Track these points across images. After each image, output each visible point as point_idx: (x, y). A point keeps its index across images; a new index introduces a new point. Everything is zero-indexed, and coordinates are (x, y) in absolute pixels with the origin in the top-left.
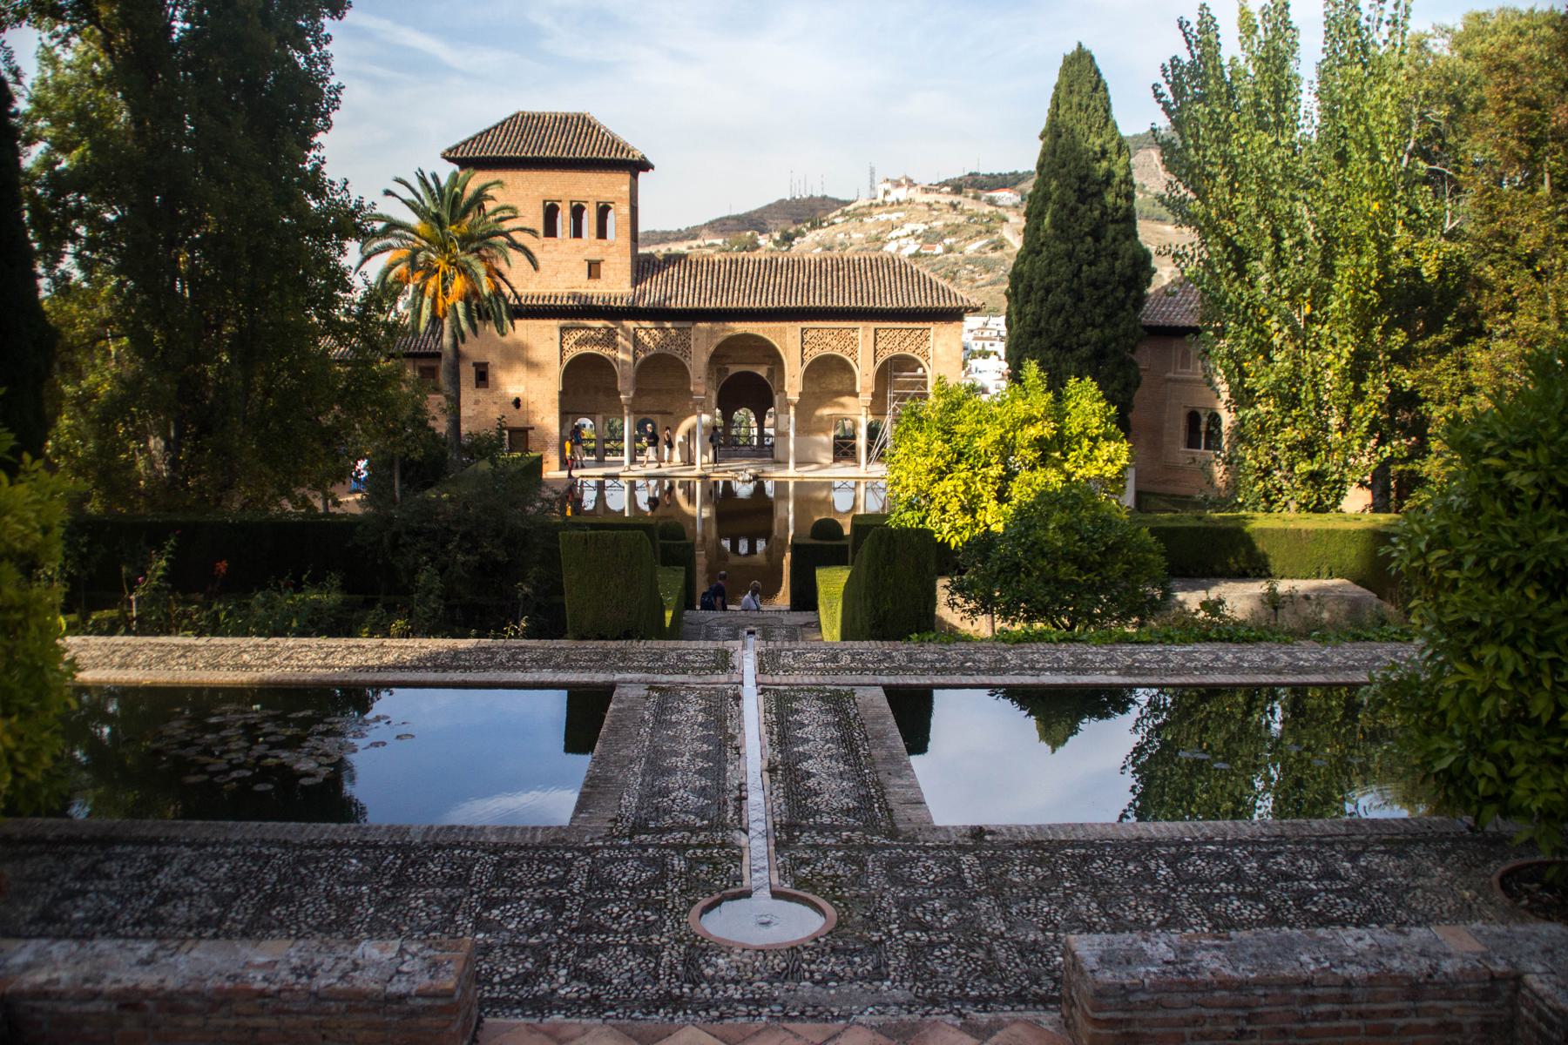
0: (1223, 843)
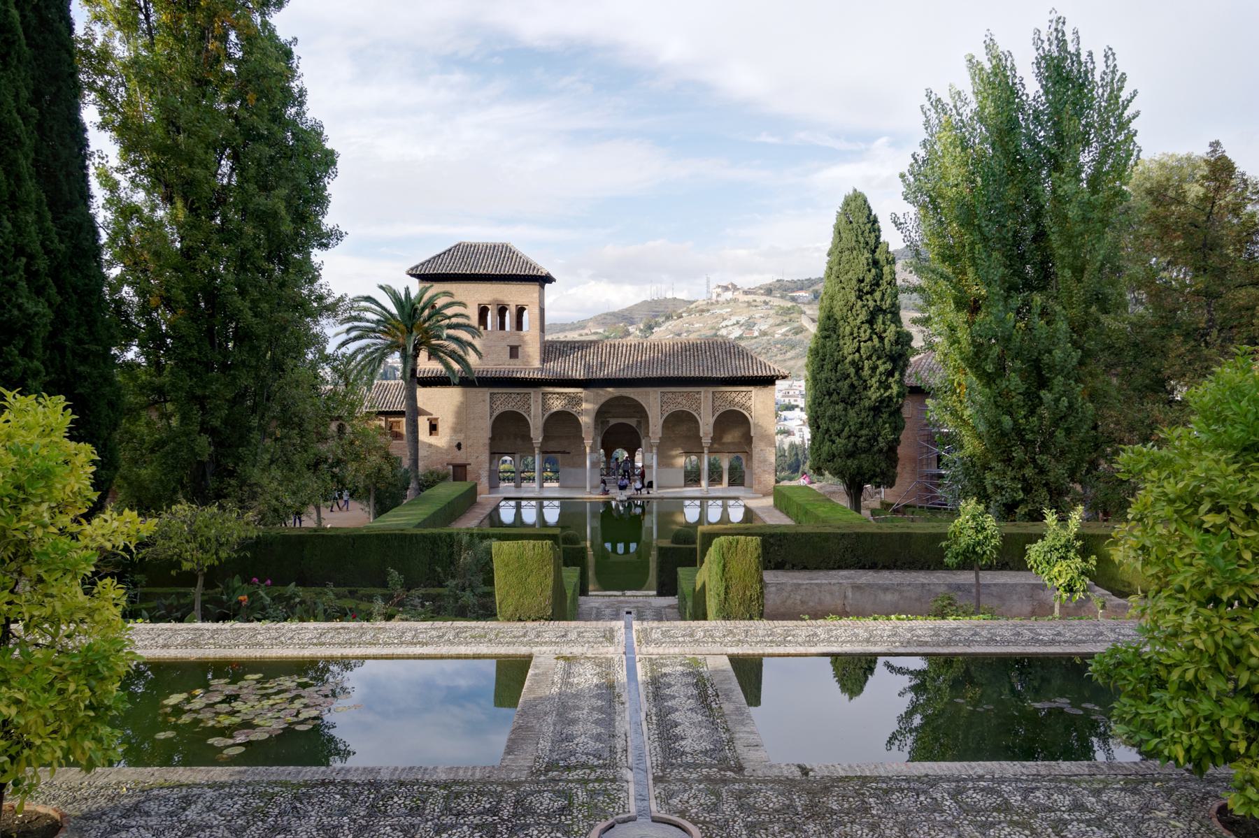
0: (993, 779)
